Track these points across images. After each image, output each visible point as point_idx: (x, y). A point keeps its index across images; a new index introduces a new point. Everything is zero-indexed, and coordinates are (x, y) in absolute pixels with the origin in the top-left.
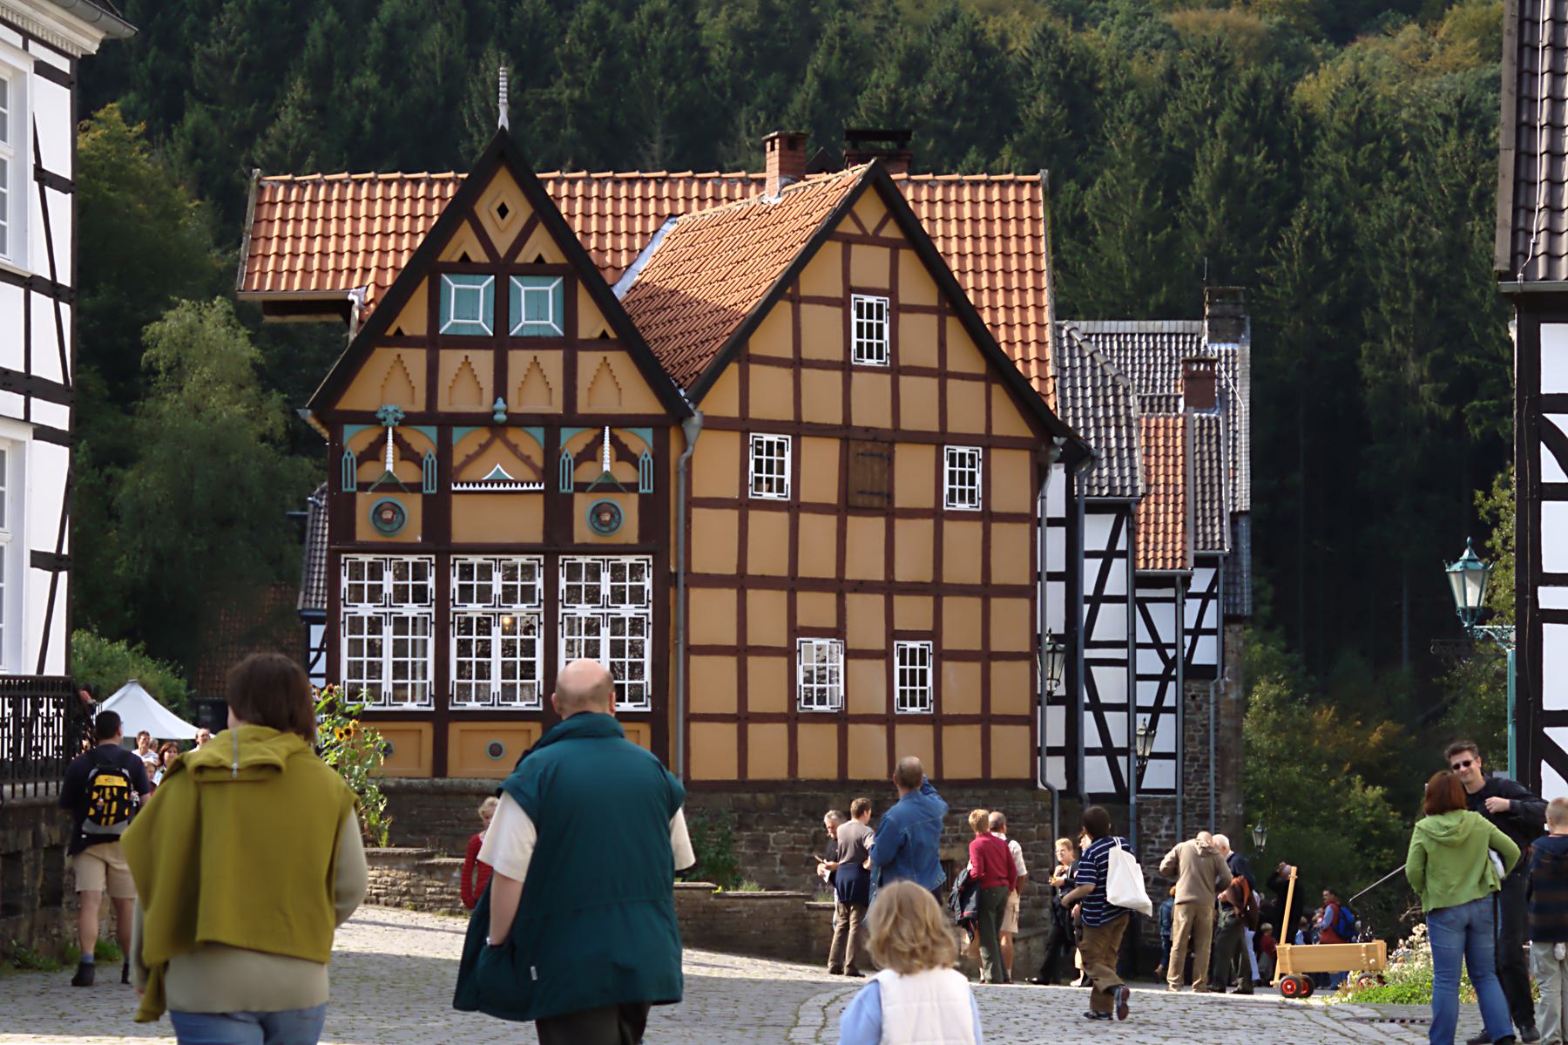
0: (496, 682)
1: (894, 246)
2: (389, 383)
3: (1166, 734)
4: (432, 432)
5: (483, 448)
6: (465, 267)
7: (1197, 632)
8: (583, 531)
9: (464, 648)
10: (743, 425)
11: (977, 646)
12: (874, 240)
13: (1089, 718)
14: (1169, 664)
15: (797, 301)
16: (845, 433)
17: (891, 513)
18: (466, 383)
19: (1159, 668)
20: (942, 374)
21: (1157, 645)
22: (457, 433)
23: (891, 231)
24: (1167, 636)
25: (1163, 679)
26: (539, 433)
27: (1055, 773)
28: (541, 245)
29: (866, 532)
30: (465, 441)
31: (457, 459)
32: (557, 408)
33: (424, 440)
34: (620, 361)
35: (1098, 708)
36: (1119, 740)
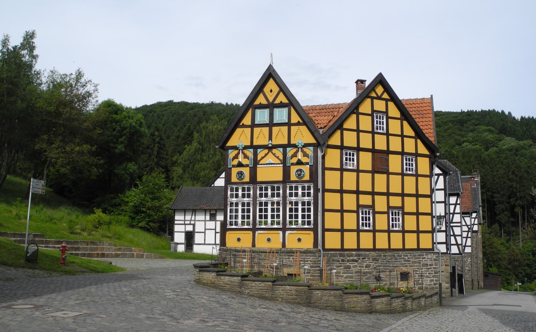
0: (269, 220)
1: (386, 100)
2: (240, 138)
3: (469, 243)
4: (252, 150)
5: (266, 155)
6: (261, 107)
7: (474, 224)
8: (293, 177)
9: (261, 210)
10: (342, 147)
11: (415, 211)
12: (379, 98)
13: (452, 238)
14: (469, 229)
15: (358, 114)
16: (373, 151)
17: (388, 173)
18: (261, 137)
19: (467, 230)
20: (402, 136)
21: (467, 225)
22: (259, 150)
23: (386, 96)
24: (468, 223)
25: (468, 232)
26: (281, 149)
27: (443, 248)
28: (281, 98)
29: (381, 179)
30: (261, 153)
31: (259, 158)
32: (286, 142)
33: (250, 153)
34: (304, 128)
35: (455, 236)
36: (459, 242)
